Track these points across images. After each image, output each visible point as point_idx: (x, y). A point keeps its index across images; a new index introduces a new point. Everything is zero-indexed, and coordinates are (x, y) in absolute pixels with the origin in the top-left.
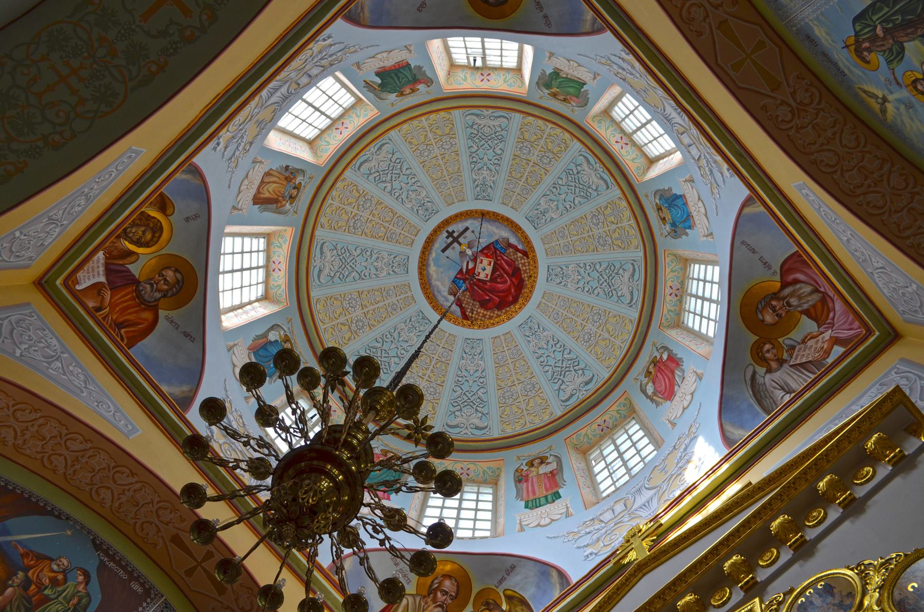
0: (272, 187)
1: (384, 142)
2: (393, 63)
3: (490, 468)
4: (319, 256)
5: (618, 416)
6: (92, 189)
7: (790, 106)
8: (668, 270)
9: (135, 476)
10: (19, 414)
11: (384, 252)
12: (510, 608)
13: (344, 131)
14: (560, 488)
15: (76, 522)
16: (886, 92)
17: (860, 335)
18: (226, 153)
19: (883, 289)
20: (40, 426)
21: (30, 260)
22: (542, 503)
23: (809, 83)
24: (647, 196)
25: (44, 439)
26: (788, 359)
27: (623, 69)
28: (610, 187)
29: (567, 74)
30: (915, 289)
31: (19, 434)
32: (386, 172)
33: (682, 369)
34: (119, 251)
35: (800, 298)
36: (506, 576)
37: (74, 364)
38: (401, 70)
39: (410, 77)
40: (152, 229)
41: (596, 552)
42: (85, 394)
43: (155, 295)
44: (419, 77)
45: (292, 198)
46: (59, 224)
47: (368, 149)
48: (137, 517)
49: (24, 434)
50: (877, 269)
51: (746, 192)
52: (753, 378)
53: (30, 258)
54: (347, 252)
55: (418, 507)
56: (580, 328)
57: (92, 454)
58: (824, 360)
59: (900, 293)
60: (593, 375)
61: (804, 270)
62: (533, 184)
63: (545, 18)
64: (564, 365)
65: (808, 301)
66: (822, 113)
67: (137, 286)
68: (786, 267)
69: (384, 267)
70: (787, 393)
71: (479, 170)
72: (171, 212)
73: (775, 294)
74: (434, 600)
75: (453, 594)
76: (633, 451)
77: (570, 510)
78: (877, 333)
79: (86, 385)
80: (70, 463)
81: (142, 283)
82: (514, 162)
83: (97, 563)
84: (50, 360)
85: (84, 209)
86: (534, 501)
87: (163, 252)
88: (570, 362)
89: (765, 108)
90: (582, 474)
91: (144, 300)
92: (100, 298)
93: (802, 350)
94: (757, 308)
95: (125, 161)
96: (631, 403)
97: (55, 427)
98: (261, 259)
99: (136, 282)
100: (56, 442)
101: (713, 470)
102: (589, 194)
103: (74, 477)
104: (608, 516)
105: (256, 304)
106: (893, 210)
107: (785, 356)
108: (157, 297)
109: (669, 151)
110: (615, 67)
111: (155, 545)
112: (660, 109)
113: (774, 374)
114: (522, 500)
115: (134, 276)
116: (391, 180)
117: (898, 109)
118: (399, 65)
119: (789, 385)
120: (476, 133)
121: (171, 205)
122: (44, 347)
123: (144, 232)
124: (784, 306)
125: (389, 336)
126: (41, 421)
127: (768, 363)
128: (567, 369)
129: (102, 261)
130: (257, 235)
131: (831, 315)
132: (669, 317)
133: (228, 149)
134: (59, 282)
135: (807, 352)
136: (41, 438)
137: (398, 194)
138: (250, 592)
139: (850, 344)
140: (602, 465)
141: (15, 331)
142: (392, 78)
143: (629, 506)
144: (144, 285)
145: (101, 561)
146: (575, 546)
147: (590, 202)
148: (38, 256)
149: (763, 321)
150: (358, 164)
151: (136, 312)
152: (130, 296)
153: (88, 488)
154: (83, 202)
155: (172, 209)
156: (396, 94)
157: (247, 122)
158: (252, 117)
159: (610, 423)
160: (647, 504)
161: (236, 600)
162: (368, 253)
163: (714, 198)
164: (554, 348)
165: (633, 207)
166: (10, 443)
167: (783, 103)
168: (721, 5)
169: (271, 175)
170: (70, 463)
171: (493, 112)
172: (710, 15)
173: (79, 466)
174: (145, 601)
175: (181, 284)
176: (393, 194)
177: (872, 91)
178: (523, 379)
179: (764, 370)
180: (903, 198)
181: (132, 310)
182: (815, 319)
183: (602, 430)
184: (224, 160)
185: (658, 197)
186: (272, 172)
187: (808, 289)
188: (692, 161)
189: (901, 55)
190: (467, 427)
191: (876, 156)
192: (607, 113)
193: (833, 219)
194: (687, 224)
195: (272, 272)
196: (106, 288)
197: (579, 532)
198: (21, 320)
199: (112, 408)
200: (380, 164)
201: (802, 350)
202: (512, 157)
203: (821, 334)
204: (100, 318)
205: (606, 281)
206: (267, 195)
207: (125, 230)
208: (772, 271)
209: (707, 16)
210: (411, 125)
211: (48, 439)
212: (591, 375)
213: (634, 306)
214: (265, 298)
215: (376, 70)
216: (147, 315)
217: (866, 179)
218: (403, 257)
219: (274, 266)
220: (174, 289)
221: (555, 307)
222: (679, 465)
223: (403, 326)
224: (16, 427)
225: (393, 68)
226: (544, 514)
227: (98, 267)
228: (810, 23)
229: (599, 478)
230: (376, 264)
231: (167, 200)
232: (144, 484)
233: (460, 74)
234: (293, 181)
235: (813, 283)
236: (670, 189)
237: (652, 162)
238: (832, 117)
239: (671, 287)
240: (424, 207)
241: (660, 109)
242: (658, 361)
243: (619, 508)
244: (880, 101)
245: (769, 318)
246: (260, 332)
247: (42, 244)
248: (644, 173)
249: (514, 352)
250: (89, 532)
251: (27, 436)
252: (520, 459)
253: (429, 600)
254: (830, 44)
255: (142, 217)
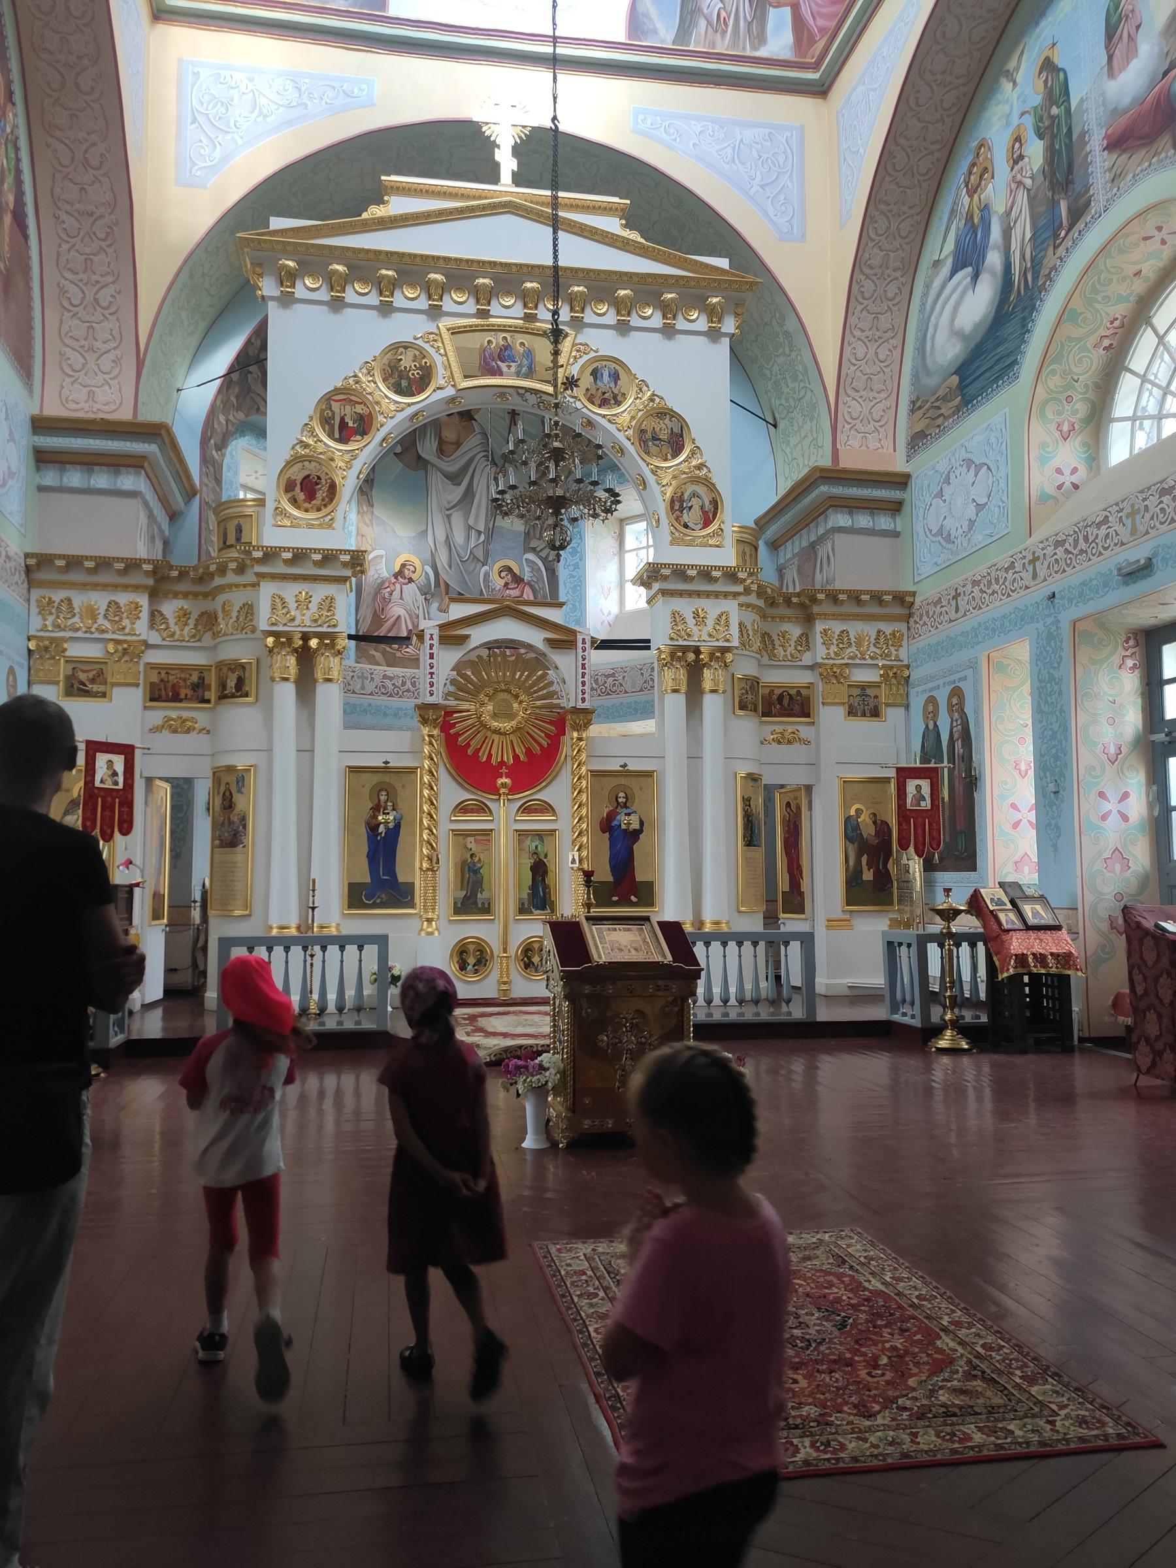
34: (873, 1244)
189: (806, 34)
224: (92, 294)
232: (63, 336)
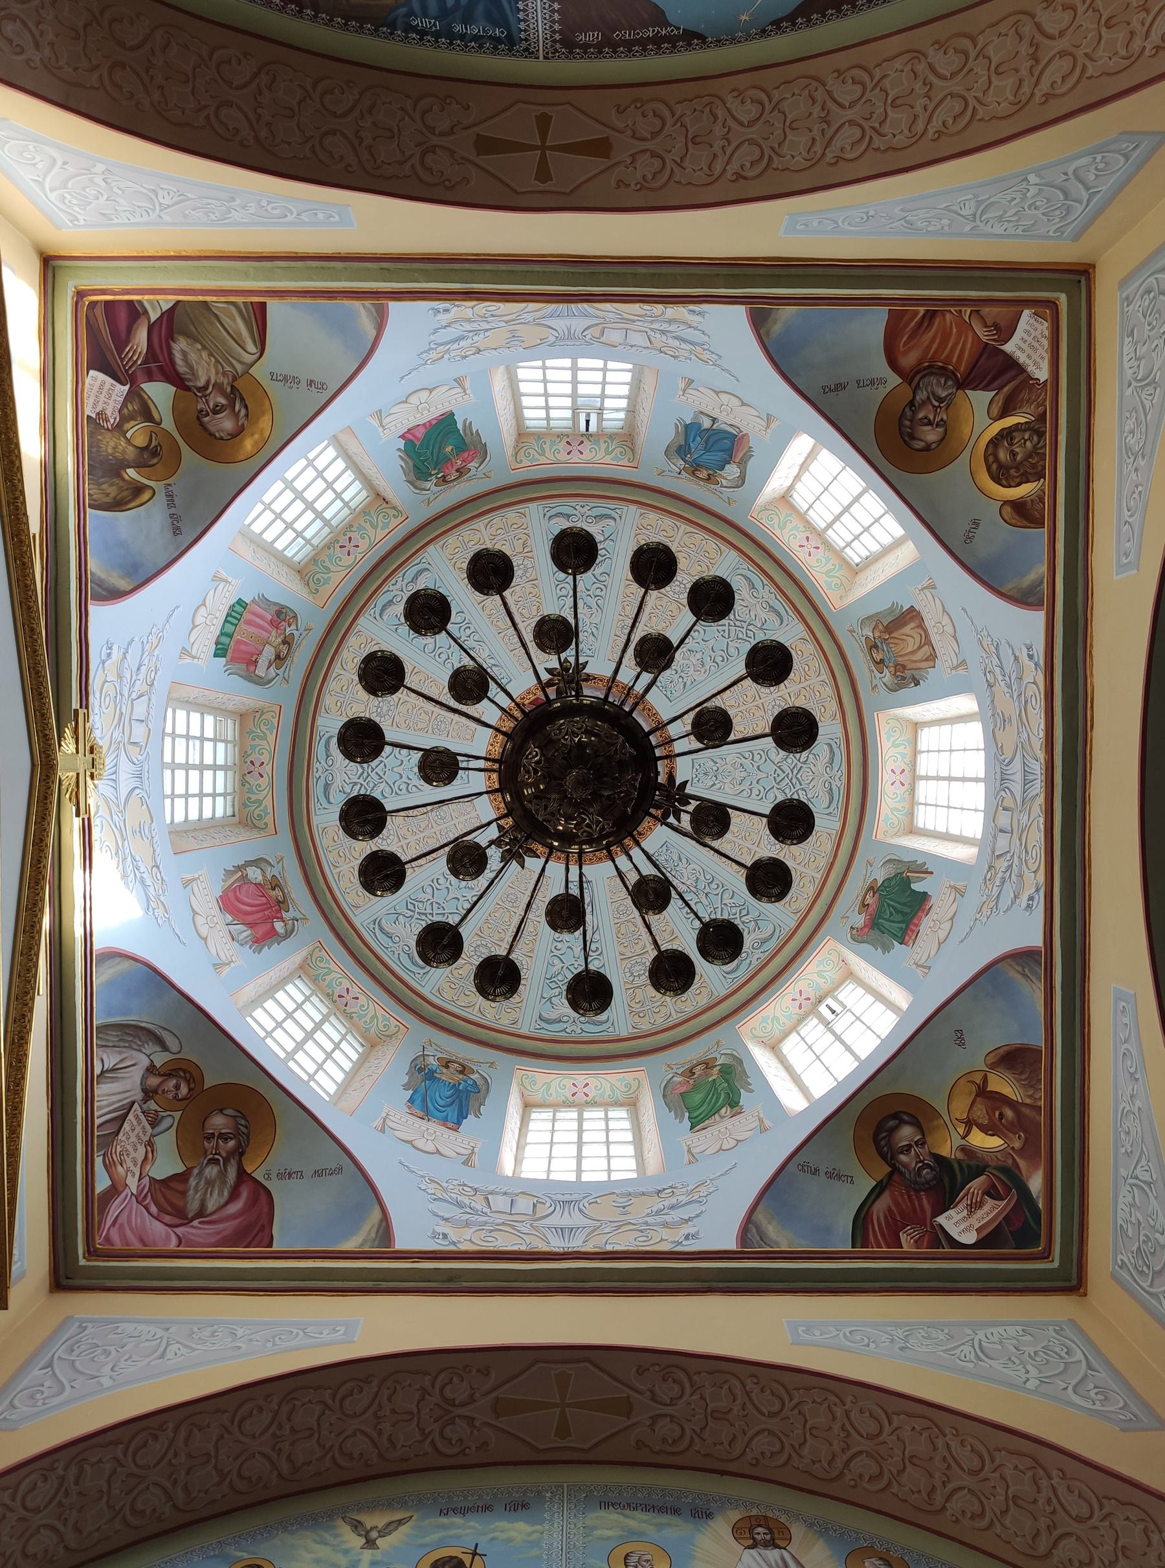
0: (911, 644)
1: (834, 805)
2: (921, 928)
3: (327, 581)
4: (771, 603)
5: (254, 797)
6: (1136, 470)
7: (462, 1405)
8: (380, 1012)
9: (734, 177)
10: (958, 106)
11: (702, 679)
12: (123, 479)
13: (893, 777)
14: (227, 662)
15: (749, 38)
16: (377, 1555)
17: (99, 1229)
18: (1011, 652)
19: (135, 1325)
20: (916, 117)
21: (1127, 298)
22: (227, 625)
23: (467, 1451)
24: (492, 1064)
25: (894, 105)
26: (145, 1107)
27: (672, 1207)
28: (539, 1022)
29: (722, 1117)
30: (103, 1380)
31: (932, 78)
32: (795, 771)
33: (246, 943)
35: (210, 1183)
36: (173, 510)
37: (946, 228)
38: (904, 926)
39: (886, 924)
40: (1008, 468)
41: (107, 663)
42: (897, 211)
43: (925, 393)
44: (874, 933)
45: (873, 647)
46: (1134, 384)
47: (844, 779)
48: (679, 124)
49: (925, 84)
50: (168, 1345)
51: (402, 1243)
52: (160, 1042)
53: (1129, 301)
54: (745, 637)
55: (357, 459)
56: (401, 832)
57: (814, 149)
58: (104, 1155)
59: (111, 1348)
60: (329, 802)
61: (239, 1220)
62: (623, 926)
63: (815, 1169)
64: (373, 774)
65: (196, 1192)
66: (419, 1438)
67: (956, 381)
68: (263, 1198)
69: (686, 662)
70: (102, 1072)
71: (698, 879)
72: (1004, 513)
73: (242, 1154)
74: (218, 387)
75: (206, 419)
76: (195, 731)
77: (189, 660)
78: (82, 1262)
79: (906, 222)
80: (830, 105)
81: (954, 390)
82: (669, 929)
83: (671, 18)
84: (981, 208)
85: (1122, 431)
86: (239, 617)
87: (966, 454)
88: (371, 785)
89: (485, 1372)
90: (219, 700)
91: (932, 374)
92: (989, 322)
93: (141, 1134)
94: (244, 1118)
95: (1128, 545)
96: (256, 827)
97: (894, 136)
98: (925, 790)
99: (964, 383)
100: (875, 116)
101: (87, 910)
102: (553, 985)
103: (807, 92)
104: (140, 709)
105: (789, 483)
106: (226, 1436)
107: (152, 1105)
108: (920, 392)
109: (521, 1162)
110: (684, 1199)
111: (621, 110)
112: (586, 1205)
113: (142, 1072)
114: (253, 601)
115: (974, 389)
116: (779, 767)
117: (346, 1552)
118: (913, 931)
119: (112, 1082)
120: (743, 919)
121: (1013, 521)
122: (1005, 212)
123: (1014, 455)
124: (216, 1154)
125: (598, 592)
126: (920, 127)
127: (162, 1075)
128: (365, 775)
129: (1031, 368)
130: (872, 560)
131: (154, 1209)
132: (322, 965)
133: (1012, 659)
134: (1063, 299)
135: (133, 1139)
136: (898, 102)
137: (755, 759)
138: (447, 183)
139: (97, 1205)
140: (209, 733)
141: (1062, 197)
142: (904, 904)
143: (129, 747)
144: (950, 391)
145: (667, 24)
146: (136, 639)
147: (543, 978)
148: (1122, 313)
149: (221, 1111)
150: (836, 750)
151: (929, 347)
152: (954, 360)
153: (776, 96)
154: (1131, 441)
155: (1007, 518)
156: (879, 884)
157: (1020, 711)
158: (1022, 723)
159: (252, 780)
160: (113, 777)
161: (452, 152)
162: (719, 659)
163: (424, 1177)
164: (404, 779)
165: (493, 1033)
166: (931, 52)
167: (472, 1400)
168: (652, 1426)
169: (927, 660)
170: (830, 105)
171: (750, 964)
172: (651, 1403)
173: (815, 115)
174: (560, 32)
175: (906, 438)
176: (762, 753)
177: (395, 1534)
178: (400, 708)
179: (158, 1064)
180: (231, 1459)
181: (935, 346)
182: (165, 1182)
183: (252, 762)
184: (1003, 641)
185: (480, 1082)
186: (931, 664)
187: (211, 1205)
188: (491, 1188)
190: (402, 591)
191: (309, 1464)
192: (631, 1104)
193: (277, 1339)
194: (418, 1102)
195: (808, 534)
196: (993, 340)
197: (151, 655)
198: (1067, 214)
199: (846, 226)
200: (811, 774)
201: (141, 1134)
202: (677, 933)
203: (141, 1174)
204: (963, 309)
205: (432, 914)
206: (907, 629)
207: (1041, 434)
208: (273, 1176)
209: (653, 1398)
210: (824, 855)
211: (889, 109)
212: (332, 800)
213: (371, 926)
214: (785, 498)
215: (933, 901)
216: (909, 360)
217: (293, 1430)
218: (676, 694)
219: (813, 543)
220: (908, 423)
221: (453, 822)
222: (129, 859)
223: (595, 620)
225: (915, 921)
226: (212, 620)
227: (1029, 357)
228: (539, 1528)
229: (195, 717)
230: (698, 656)
231: (1025, 523)
232: (713, 178)
233: (832, 975)
234: (892, 669)
235: (214, 1217)
236: (478, 1114)
237: (528, 1106)
238: (403, 1446)
239: (357, 998)
240: (711, 774)
241: (586, 1205)
242: (279, 911)
243: (139, 733)
244: (374, 1534)
245: (218, 1122)
246: (751, 465)
247: (1131, 334)
248: (522, 1085)
249: (443, 726)
250: (719, 43)
251: (918, 86)
252: (306, 630)
253: (226, 382)
254: (494, 1531)
255: (1033, 471)
